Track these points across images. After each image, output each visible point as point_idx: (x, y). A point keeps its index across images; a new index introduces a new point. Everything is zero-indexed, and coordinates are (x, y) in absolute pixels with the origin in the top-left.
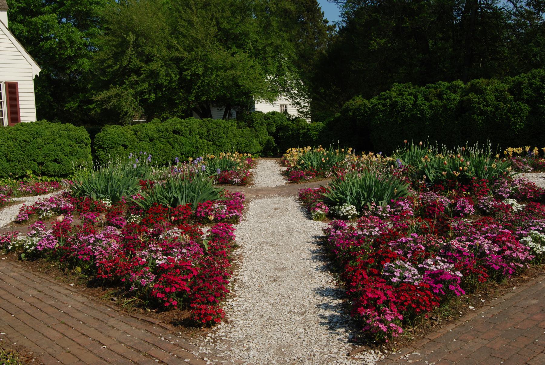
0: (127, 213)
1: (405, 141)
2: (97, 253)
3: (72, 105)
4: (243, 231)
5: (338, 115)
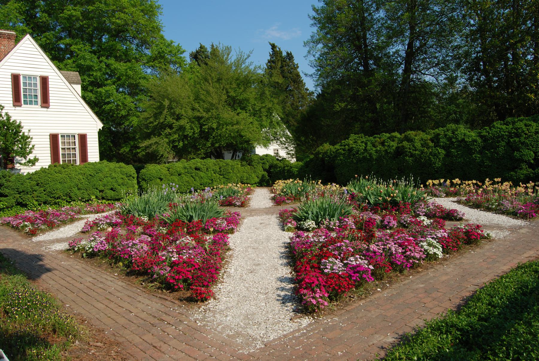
0: (158, 227)
1: (356, 176)
2: (133, 253)
3: (125, 149)
4: (236, 239)
5: (312, 157)
